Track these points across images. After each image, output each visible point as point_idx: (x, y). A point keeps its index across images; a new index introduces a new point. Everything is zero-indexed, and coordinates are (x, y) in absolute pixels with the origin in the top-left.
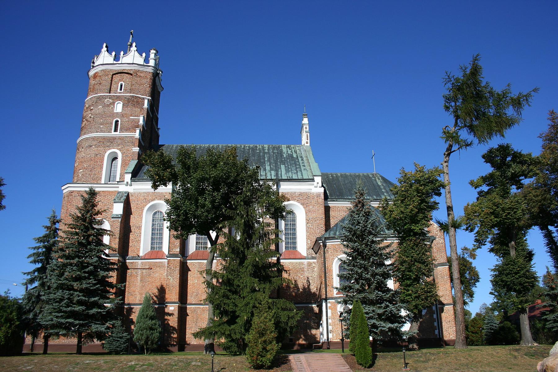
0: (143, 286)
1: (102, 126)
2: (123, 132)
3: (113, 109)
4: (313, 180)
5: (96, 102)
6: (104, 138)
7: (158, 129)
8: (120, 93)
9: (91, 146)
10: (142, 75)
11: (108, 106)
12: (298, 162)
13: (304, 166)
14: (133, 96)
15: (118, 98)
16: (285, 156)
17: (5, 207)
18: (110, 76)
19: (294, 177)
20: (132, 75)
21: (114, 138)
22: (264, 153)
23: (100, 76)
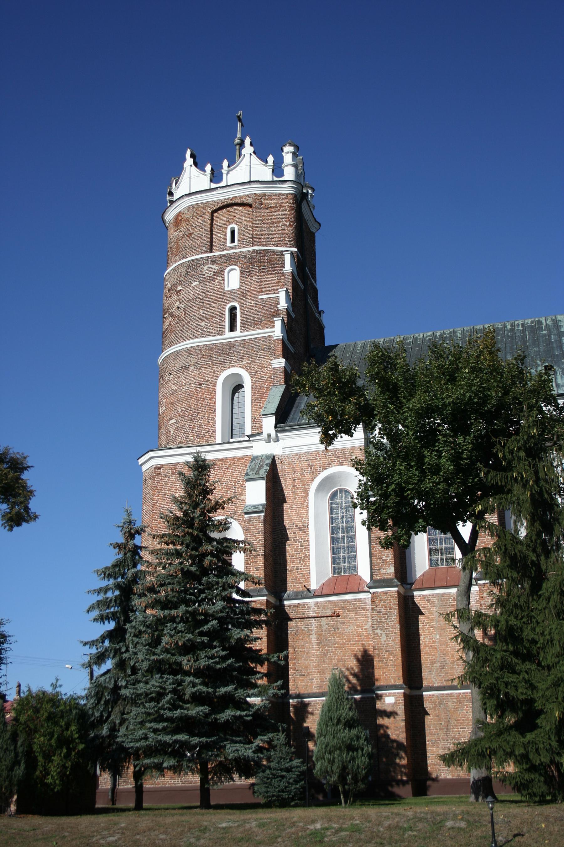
1: (203, 324)
2: (248, 330)
3: (222, 283)
5: (187, 275)
6: (211, 348)
7: (320, 313)
8: (232, 248)
9: (186, 368)
10: (272, 203)
11: (212, 279)
14: (259, 252)
15: (230, 259)
18: (208, 217)
20: (250, 206)
21: (231, 346)
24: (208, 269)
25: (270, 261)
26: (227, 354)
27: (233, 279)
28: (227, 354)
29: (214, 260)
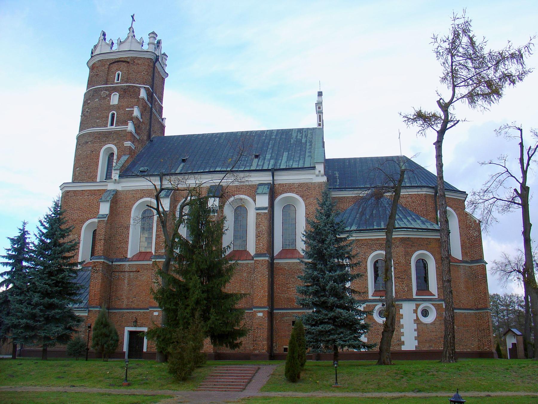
0: (131, 290)
1: (98, 121)
2: (119, 126)
3: (109, 101)
4: (314, 168)
5: (93, 95)
6: (100, 133)
7: (163, 119)
8: (117, 83)
9: (87, 143)
10: (140, 62)
11: (104, 98)
12: (306, 148)
13: (310, 152)
14: (129, 86)
15: (115, 89)
16: (292, 141)
17: (434, 144)
18: (107, 66)
19: (294, 166)
20: (128, 62)
21: (110, 133)
22: (270, 139)
23: (97, 67)
24: (103, 93)
25: (134, 91)
26: (107, 137)
27: (115, 99)
28: (107, 137)
29: (106, 89)
